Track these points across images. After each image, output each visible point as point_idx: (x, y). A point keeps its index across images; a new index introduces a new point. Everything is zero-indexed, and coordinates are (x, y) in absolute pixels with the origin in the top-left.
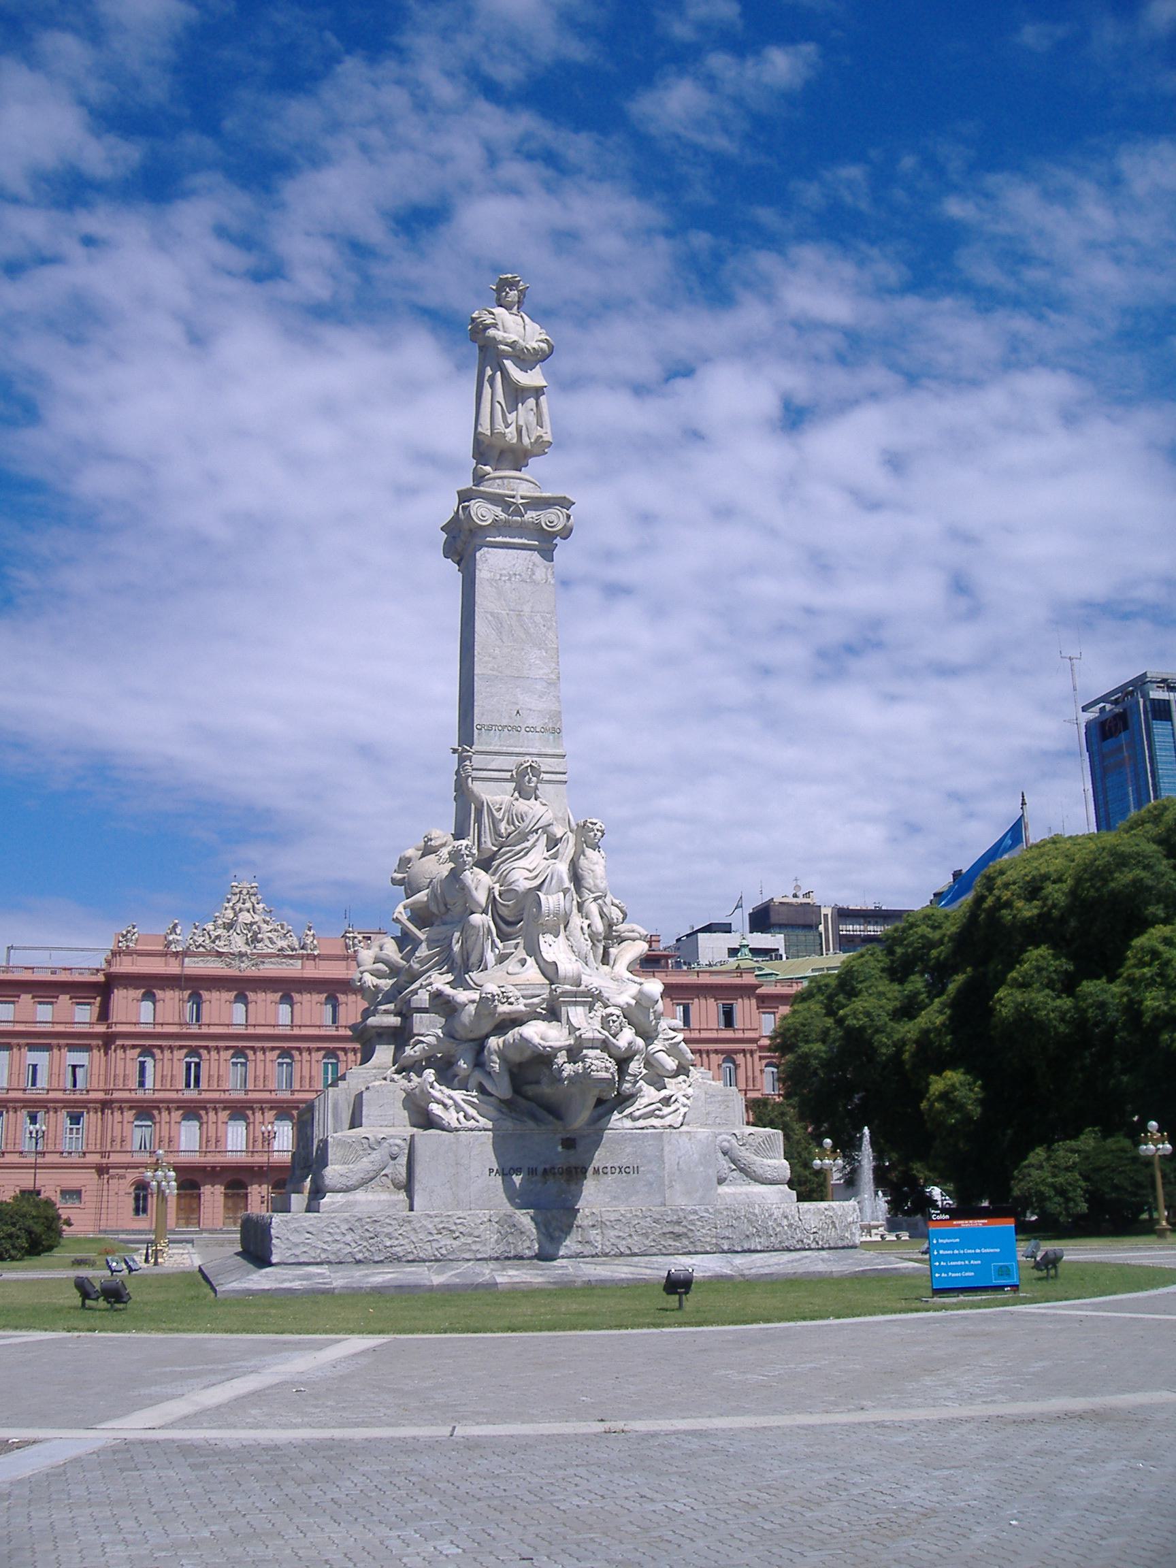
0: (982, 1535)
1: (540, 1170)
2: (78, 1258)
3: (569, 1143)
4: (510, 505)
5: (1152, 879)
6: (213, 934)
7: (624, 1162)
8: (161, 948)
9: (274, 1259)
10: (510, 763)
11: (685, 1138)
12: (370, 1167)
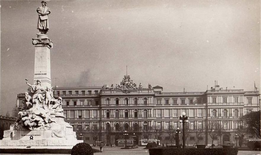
4: (39, 40)
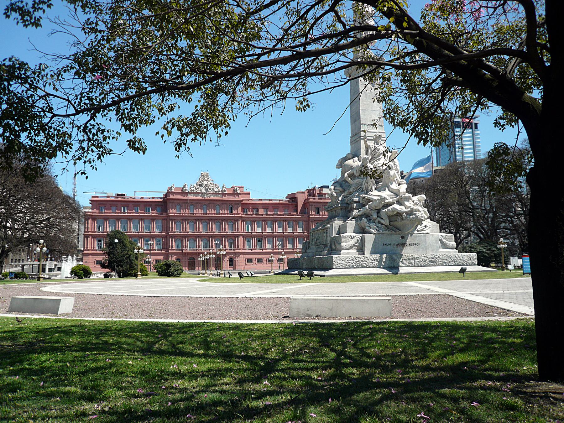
0: (525, 241)
1: (396, 244)
2: (154, 322)
3: (403, 237)
5: (411, 125)
6: (196, 187)
7: (416, 242)
8: (180, 191)
9: (334, 267)
10: (373, 135)
11: (431, 236)
12: (352, 243)
